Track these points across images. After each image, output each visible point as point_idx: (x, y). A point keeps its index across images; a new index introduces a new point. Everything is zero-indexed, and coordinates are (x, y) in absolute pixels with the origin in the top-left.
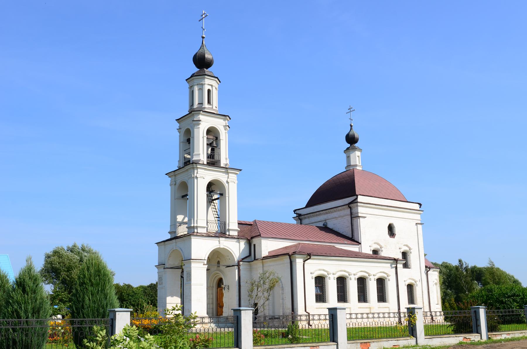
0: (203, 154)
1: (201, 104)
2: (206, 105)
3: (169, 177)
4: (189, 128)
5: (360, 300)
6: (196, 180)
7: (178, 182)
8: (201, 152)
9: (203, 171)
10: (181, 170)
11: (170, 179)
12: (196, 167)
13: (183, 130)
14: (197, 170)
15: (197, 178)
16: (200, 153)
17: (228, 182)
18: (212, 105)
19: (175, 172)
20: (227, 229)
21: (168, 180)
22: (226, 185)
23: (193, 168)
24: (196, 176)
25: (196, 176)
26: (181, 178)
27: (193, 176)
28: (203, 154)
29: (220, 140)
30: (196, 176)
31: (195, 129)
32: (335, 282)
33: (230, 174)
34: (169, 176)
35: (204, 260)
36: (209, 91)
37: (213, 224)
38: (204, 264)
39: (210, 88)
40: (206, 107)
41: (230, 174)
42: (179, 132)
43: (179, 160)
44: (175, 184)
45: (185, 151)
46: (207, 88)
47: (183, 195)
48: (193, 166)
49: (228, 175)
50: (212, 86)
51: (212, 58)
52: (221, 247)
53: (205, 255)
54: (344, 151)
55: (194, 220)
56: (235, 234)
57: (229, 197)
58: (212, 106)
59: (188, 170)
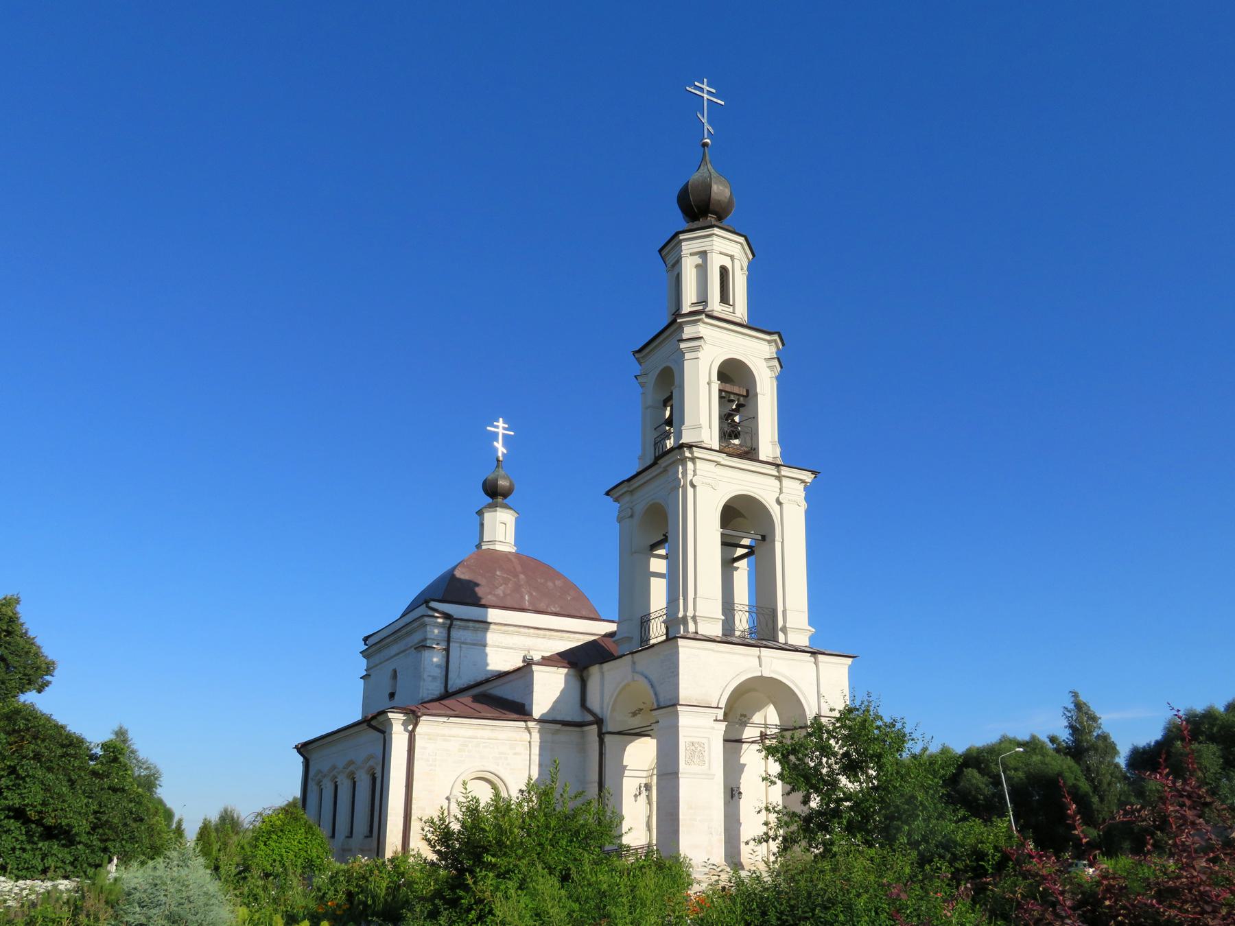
0: (710, 427)
1: (703, 301)
2: (715, 305)
3: (616, 500)
4: (673, 368)
5: (721, 301)
6: (692, 465)
7: (640, 508)
8: (704, 421)
9: (711, 466)
10: (648, 475)
11: (617, 505)
12: (690, 456)
13: (651, 379)
14: (694, 464)
15: (694, 486)
16: (700, 425)
17: (779, 503)
18: (733, 306)
19: (632, 483)
20: (779, 627)
21: (612, 508)
22: (774, 510)
23: (683, 461)
24: (692, 480)
25: (691, 481)
26: (643, 499)
27: (680, 615)
28: (710, 427)
29: (756, 395)
30: (692, 480)
31: (685, 362)
32: (694, 271)
33: (785, 481)
34: (615, 496)
35: (717, 708)
36: (724, 271)
37: (739, 612)
38: (716, 720)
39: (727, 262)
40: (715, 309)
41: (785, 481)
42: (642, 385)
43: (640, 453)
44: (632, 516)
45: (655, 429)
46: (715, 262)
47: (652, 543)
48: (681, 454)
49: (781, 482)
50: (732, 257)
51: (731, 197)
52: (765, 675)
53: (719, 693)
54: (660, 251)
55: (685, 599)
56: (802, 640)
57: (782, 543)
58: (734, 309)
59: (668, 468)
